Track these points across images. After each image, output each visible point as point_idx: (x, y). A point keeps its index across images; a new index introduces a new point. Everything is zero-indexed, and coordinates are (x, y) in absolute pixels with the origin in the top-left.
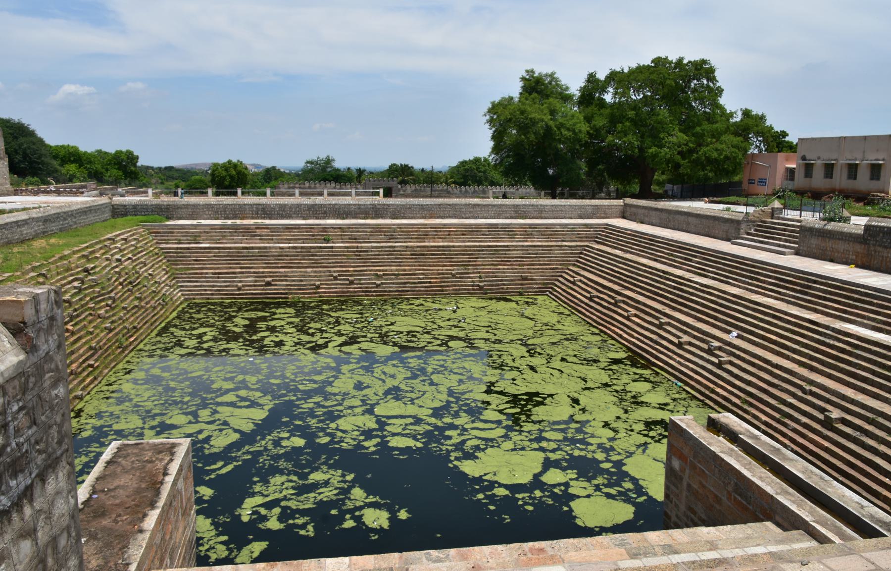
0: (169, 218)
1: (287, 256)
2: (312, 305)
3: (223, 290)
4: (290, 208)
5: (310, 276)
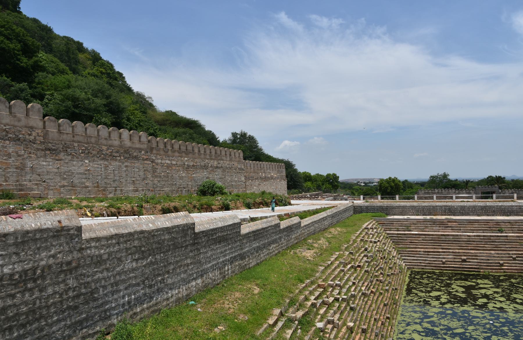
0: (388, 214)
1: (474, 241)
2: (501, 278)
3: (432, 263)
4: (468, 208)
5: (494, 257)
